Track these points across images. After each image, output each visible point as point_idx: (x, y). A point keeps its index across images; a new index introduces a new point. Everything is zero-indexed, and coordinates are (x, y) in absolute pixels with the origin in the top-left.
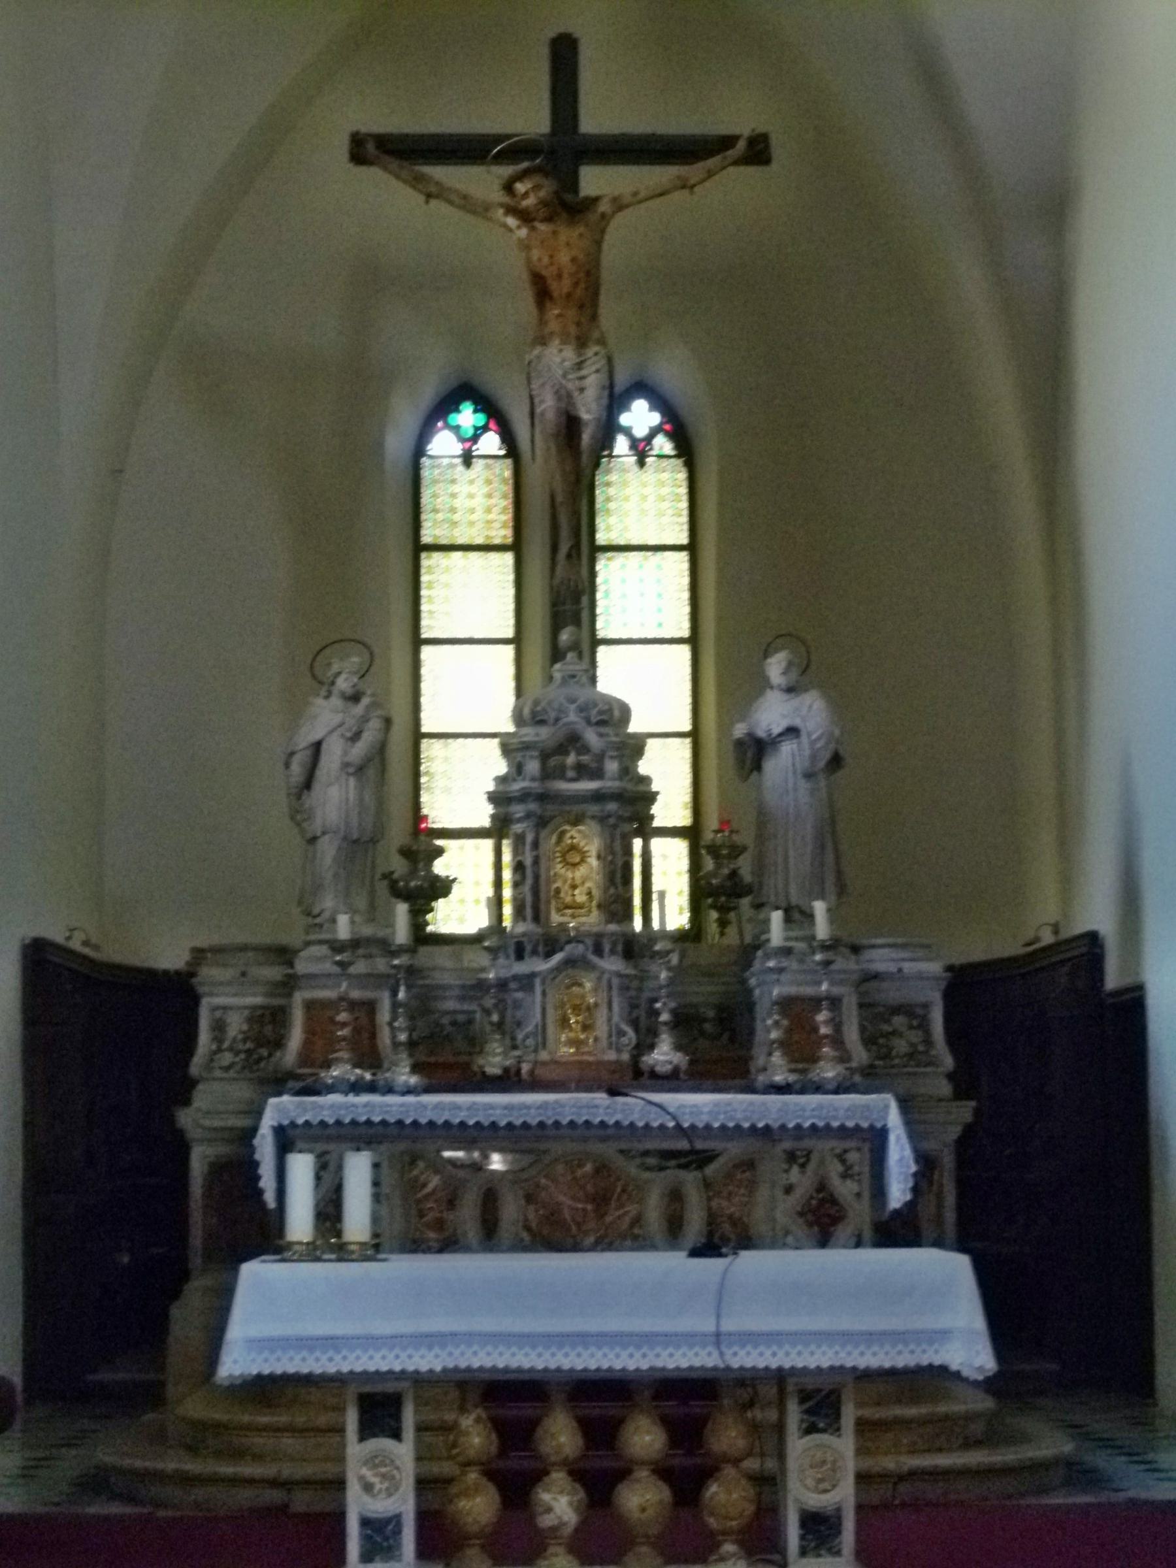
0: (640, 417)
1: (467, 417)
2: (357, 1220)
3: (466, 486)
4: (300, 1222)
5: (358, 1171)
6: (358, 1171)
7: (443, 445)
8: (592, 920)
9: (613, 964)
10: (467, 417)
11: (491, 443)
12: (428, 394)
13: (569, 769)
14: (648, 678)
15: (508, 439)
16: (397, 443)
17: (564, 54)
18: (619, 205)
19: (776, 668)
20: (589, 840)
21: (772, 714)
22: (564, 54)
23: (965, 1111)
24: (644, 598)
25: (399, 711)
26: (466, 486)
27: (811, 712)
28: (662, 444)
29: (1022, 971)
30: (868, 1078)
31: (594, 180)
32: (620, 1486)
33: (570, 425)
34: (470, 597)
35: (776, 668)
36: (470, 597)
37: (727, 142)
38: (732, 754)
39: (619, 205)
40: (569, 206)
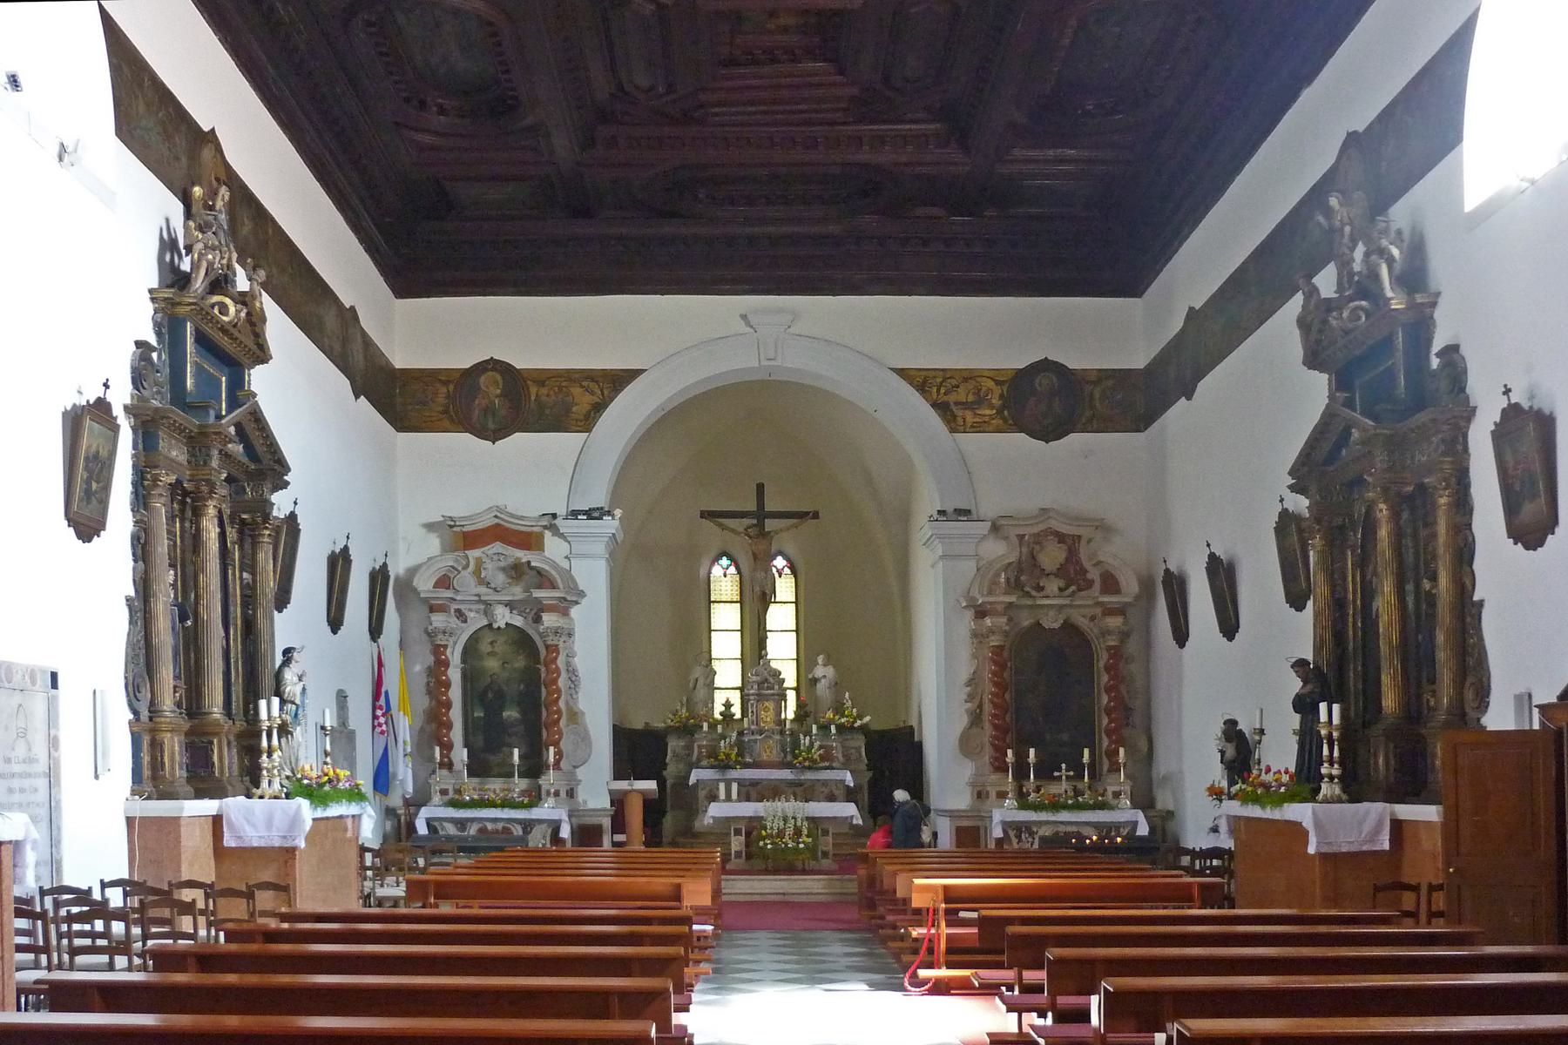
0: (780, 562)
1: (725, 561)
2: (734, 795)
3: (724, 581)
4: (722, 795)
5: (735, 786)
6: (735, 786)
7: (717, 571)
8: (772, 725)
9: (778, 737)
10: (725, 561)
11: (732, 570)
12: (713, 554)
13: (760, 681)
14: (782, 650)
15: (738, 568)
16: (703, 572)
17: (760, 488)
18: (776, 532)
19: (820, 659)
20: (770, 705)
21: (819, 671)
22: (760, 488)
23: (870, 774)
24: (781, 617)
25: (705, 649)
26: (724, 581)
27: (829, 672)
28: (787, 571)
29: (786, 774)
30: (844, 767)
31: (770, 524)
32: (763, 938)
33: (764, 594)
34: (726, 618)
35: (820, 659)
36: (726, 618)
37: (807, 513)
38: (806, 683)
39: (776, 532)
40: (763, 534)
